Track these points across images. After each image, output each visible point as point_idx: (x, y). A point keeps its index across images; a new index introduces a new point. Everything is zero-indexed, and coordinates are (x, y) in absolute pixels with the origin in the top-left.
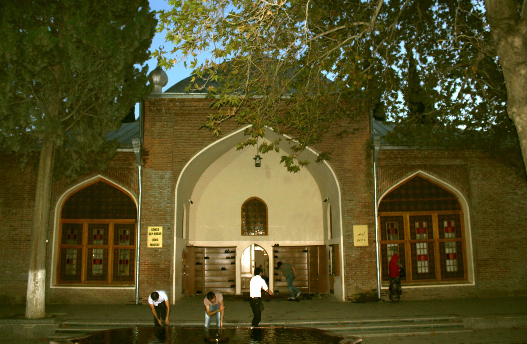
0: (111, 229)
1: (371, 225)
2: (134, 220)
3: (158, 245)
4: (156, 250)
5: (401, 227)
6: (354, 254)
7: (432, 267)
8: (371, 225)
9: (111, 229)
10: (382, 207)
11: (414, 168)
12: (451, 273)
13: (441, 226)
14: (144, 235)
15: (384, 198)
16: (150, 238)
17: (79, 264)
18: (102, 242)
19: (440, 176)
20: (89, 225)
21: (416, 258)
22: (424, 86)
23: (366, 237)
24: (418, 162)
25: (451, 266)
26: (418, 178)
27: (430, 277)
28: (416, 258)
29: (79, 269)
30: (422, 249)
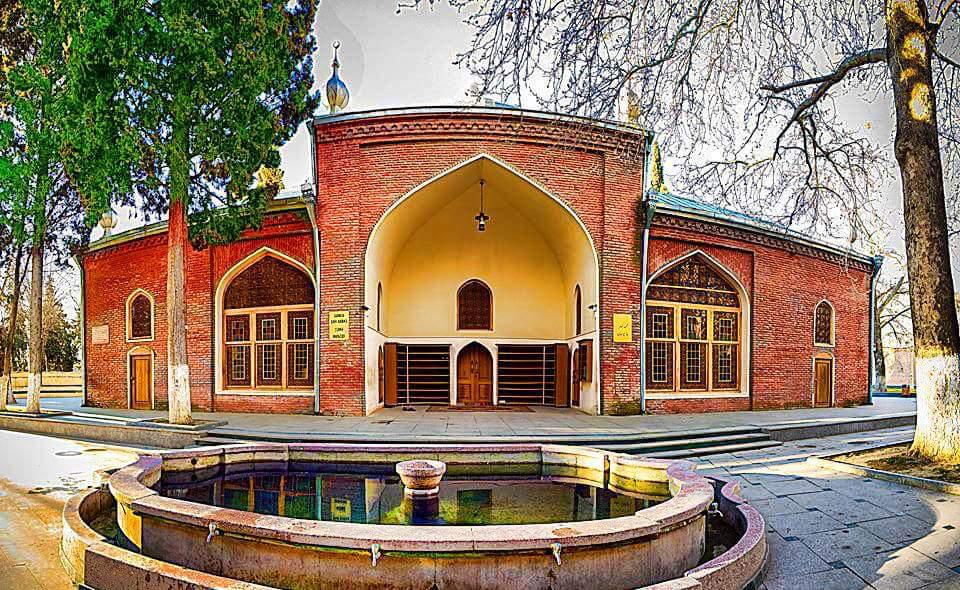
2: (312, 305)
16: (333, 327)
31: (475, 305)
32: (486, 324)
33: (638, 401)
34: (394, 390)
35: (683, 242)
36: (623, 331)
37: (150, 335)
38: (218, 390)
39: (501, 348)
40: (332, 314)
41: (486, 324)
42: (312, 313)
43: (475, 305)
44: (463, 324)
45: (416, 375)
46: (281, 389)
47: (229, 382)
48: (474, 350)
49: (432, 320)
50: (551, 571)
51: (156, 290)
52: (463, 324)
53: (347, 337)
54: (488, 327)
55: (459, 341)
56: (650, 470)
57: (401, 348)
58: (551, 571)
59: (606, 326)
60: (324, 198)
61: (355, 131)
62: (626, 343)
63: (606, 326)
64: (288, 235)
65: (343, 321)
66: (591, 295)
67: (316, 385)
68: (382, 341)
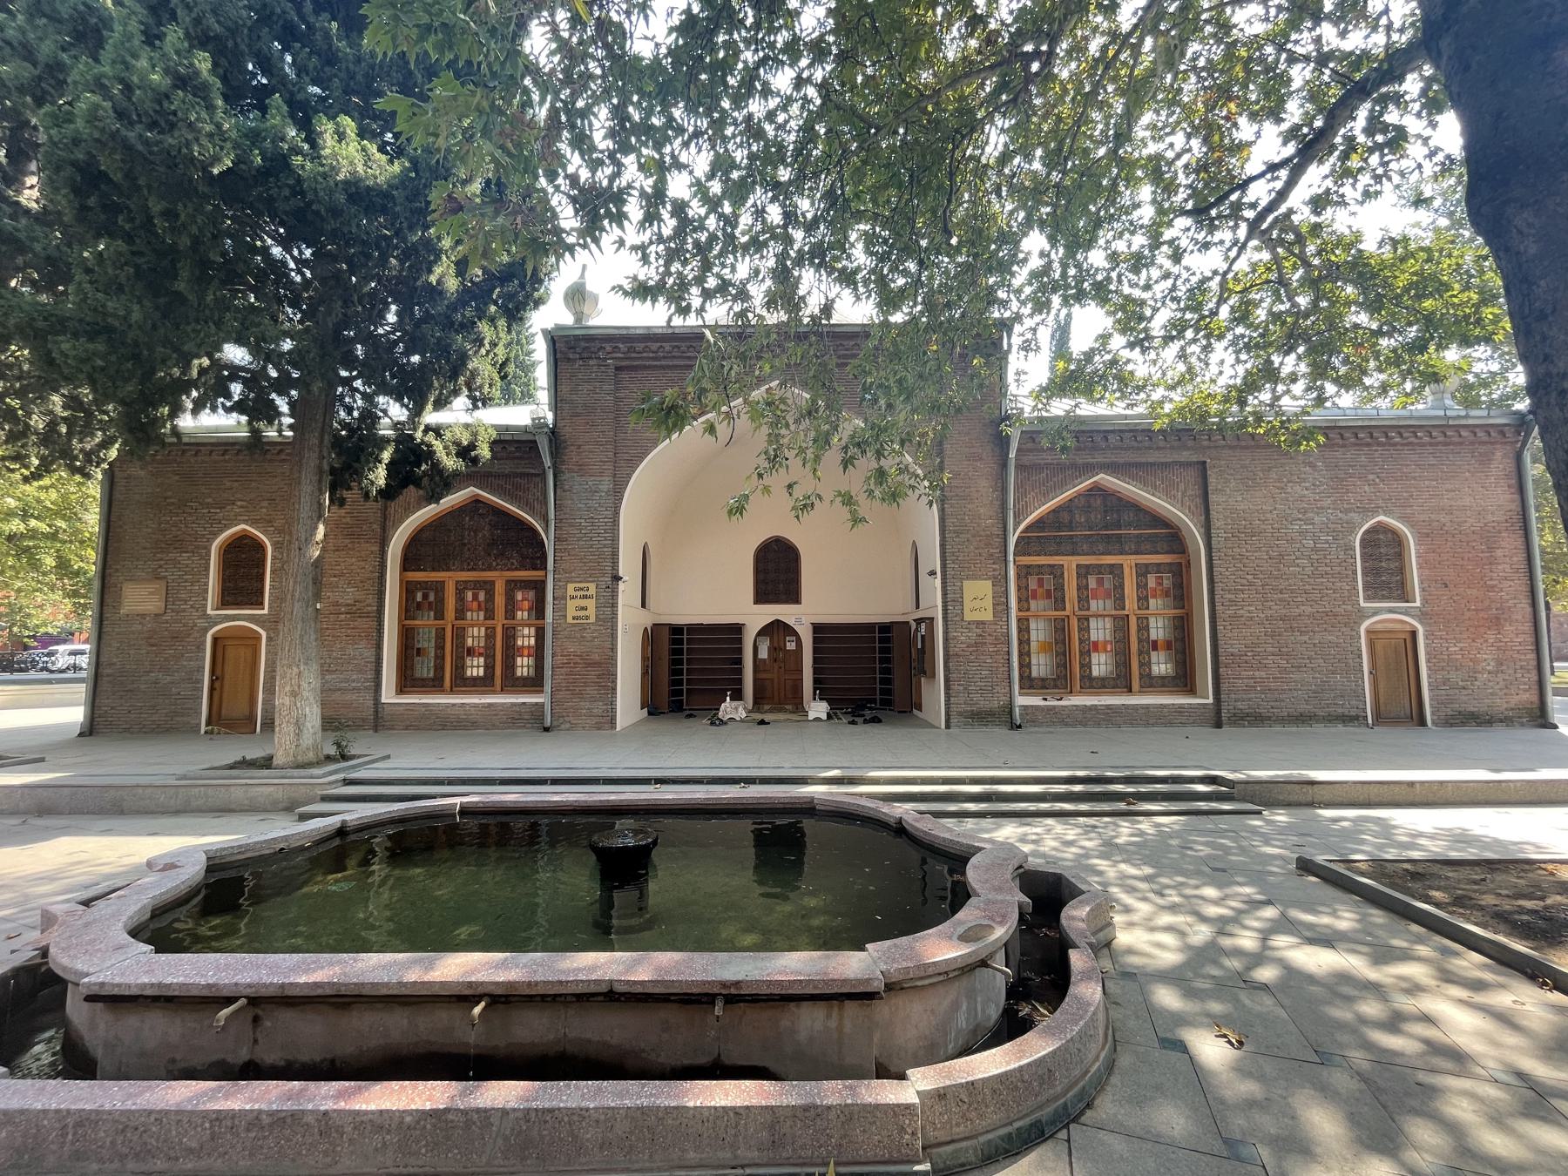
0: (500, 588)
1: (1000, 581)
2: (541, 573)
3: (587, 618)
4: (583, 628)
5: (1060, 588)
6: (963, 637)
7: (489, 668)
8: (1000, 581)
9: (500, 588)
10: (1024, 546)
11: (1091, 469)
12: (523, 678)
13: (1141, 586)
14: (560, 599)
15: (1026, 530)
16: (571, 606)
17: (440, 658)
18: (482, 614)
19: (1144, 484)
20: (508, 582)
21: (1090, 648)
22: (423, 356)
23: (988, 603)
24: (1099, 458)
25: (1161, 666)
26: (1097, 490)
27: (483, 684)
28: (1090, 648)
29: (439, 668)
30: (1100, 631)
31: (777, 570)
32: (791, 595)
33: (1009, 708)
34: (665, 688)
35: (1074, 466)
36: (977, 604)
37: (262, 603)
38: (388, 695)
39: (818, 628)
40: (571, 587)
41: (791, 595)
42: (544, 582)
43: (777, 570)
44: (763, 595)
45: (690, 672)
46: (494, 692)
47: (407, 682)
48: (777, 629)
49: (719, 593)
50: (340, 142)
51: (280, 531)
52: (763, 595)
53: (593, 619)
54: (796, 599)
55: (756, 617)
56: (104, 636)
57: (676, 630)
58: (340, 142)
59: (951, 600)
60: (566, 431)
61: (609, 349)
62: (983, 623)
63: (951, 600)
64: (508, 476)
65: (585, 597)
66: (932, 558)
67: (548, 687)
68: (647, 619)
